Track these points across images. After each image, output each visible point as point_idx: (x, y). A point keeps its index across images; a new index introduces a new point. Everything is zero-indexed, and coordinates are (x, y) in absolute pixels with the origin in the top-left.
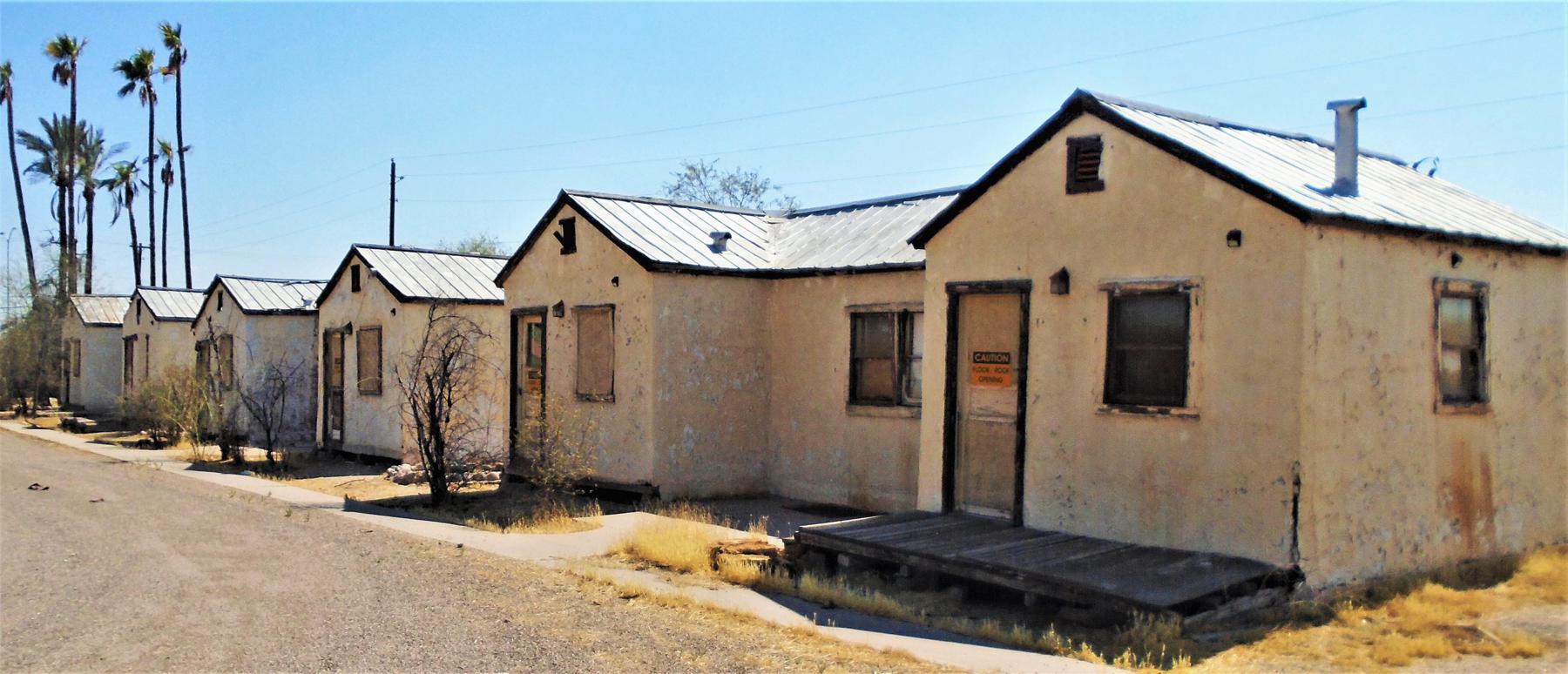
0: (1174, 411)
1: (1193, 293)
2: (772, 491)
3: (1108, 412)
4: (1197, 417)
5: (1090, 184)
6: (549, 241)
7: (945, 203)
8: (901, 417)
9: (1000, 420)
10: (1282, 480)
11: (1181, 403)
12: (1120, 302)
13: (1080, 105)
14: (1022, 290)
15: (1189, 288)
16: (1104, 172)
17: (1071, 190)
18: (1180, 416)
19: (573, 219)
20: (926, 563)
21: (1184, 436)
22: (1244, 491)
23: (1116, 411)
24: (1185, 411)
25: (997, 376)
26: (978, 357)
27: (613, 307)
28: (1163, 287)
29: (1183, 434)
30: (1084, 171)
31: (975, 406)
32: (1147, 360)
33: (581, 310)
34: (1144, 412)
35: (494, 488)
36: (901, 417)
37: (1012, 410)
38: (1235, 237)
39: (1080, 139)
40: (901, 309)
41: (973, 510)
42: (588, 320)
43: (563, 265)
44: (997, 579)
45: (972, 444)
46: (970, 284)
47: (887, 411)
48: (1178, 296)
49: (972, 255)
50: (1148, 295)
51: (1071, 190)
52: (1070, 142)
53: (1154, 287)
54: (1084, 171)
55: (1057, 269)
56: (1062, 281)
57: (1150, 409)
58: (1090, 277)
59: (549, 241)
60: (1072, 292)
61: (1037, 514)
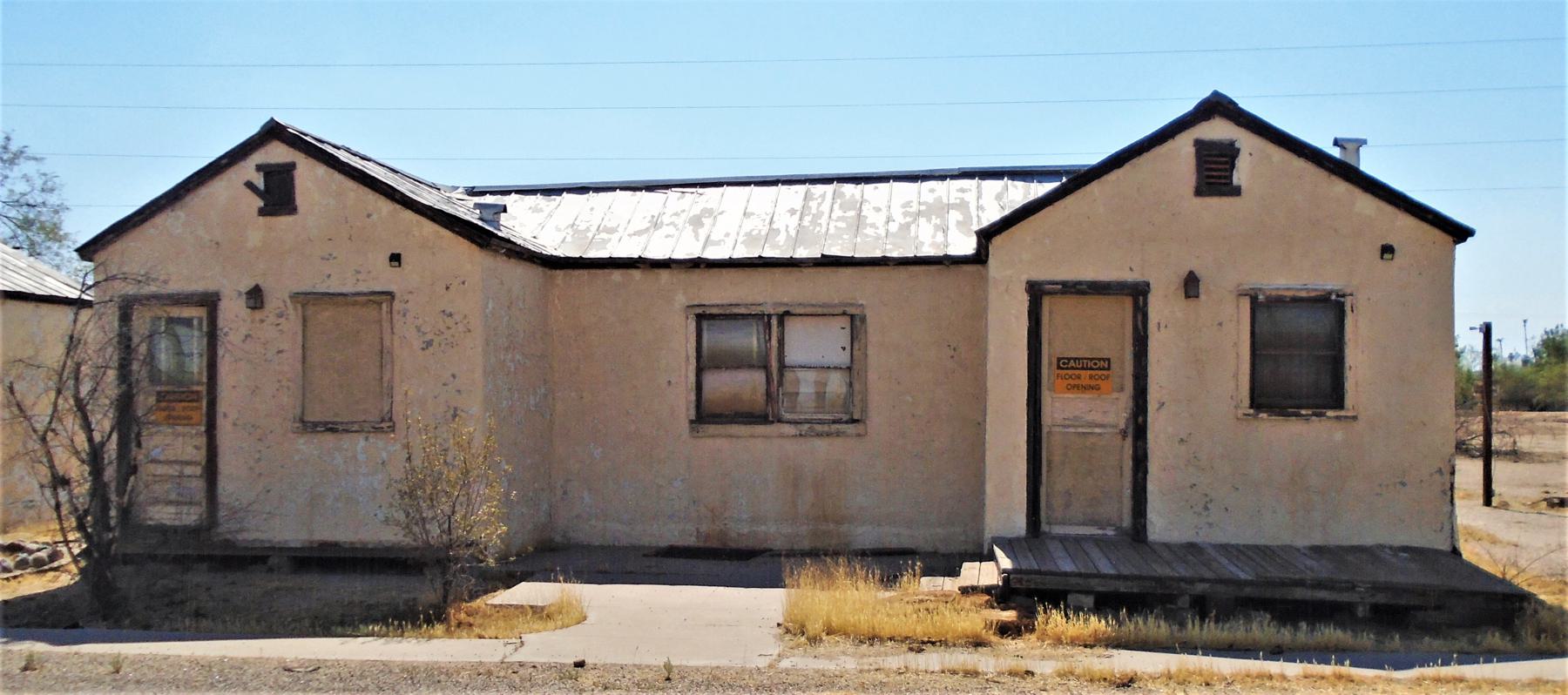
0: (1330, 413)
1: (1348, 302)
2: (558, 539)
3: (1255, 416)
4: (1355, 418)
5: (1224, 188)
6: (232, 191)
7: (1021, 193)
8: (782, 436)
9: (1097, 430)
10: (1440, 471)
11: (1339, 404)
12: (1262, 305)
13: (1216, 107)
14: (1138, 293)
15: (1343, 296)
16: (1238, 178)
17: (1199, 192)
18: (1338, 418)
19: (290, 168)
20: (1221, 588)
21: (1339, 436)
22: (1403, 484)
23: (1264, 415)
24: (1342, 413)
25: (1093, 383)
26: (1063, 363)
27: (390, 295)
28: (1313, 294)
29: (1338, 434)
30: (277, 194)
31: (1059, 417)
32: (1298, 360)
33: (307, 300)
34: (1298, 415)
35: (65, 580)
36: (782, 436)
37: (201, 456)
38: (1387, 250)
39: (277, 165)
40: (781, 310)
41: (1058, 530)
42: (324, 315)
43: (260, 231)
44: (1323, 595)
45: (1057, 459)
46: (1064, 284)
47: (760, 429)
48: (1333, 306)
49: (1077, 248)
50: (1296, 300)
51: (1199, 192)
52: (1200, 145)
53: (1304, 294)
54: (1215, 169)
55: (1184, 273)
56: (1191, 285)
57: (1303, 412)
58: (1222, 283)
59: (232, 191)
60: (1203, 297)
61: (1162, 525)
